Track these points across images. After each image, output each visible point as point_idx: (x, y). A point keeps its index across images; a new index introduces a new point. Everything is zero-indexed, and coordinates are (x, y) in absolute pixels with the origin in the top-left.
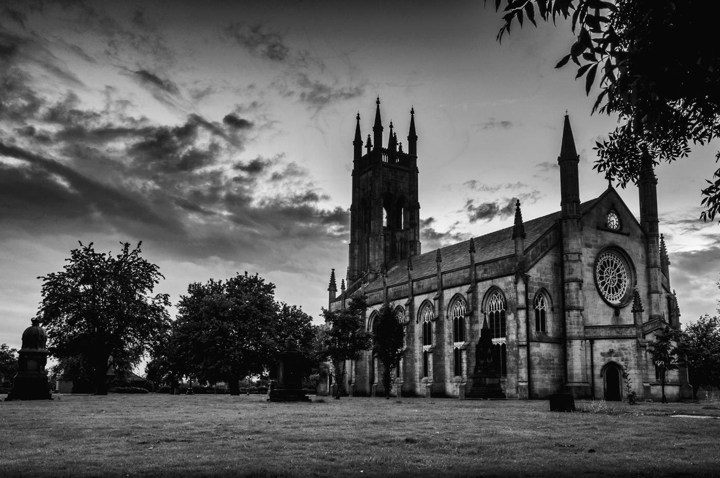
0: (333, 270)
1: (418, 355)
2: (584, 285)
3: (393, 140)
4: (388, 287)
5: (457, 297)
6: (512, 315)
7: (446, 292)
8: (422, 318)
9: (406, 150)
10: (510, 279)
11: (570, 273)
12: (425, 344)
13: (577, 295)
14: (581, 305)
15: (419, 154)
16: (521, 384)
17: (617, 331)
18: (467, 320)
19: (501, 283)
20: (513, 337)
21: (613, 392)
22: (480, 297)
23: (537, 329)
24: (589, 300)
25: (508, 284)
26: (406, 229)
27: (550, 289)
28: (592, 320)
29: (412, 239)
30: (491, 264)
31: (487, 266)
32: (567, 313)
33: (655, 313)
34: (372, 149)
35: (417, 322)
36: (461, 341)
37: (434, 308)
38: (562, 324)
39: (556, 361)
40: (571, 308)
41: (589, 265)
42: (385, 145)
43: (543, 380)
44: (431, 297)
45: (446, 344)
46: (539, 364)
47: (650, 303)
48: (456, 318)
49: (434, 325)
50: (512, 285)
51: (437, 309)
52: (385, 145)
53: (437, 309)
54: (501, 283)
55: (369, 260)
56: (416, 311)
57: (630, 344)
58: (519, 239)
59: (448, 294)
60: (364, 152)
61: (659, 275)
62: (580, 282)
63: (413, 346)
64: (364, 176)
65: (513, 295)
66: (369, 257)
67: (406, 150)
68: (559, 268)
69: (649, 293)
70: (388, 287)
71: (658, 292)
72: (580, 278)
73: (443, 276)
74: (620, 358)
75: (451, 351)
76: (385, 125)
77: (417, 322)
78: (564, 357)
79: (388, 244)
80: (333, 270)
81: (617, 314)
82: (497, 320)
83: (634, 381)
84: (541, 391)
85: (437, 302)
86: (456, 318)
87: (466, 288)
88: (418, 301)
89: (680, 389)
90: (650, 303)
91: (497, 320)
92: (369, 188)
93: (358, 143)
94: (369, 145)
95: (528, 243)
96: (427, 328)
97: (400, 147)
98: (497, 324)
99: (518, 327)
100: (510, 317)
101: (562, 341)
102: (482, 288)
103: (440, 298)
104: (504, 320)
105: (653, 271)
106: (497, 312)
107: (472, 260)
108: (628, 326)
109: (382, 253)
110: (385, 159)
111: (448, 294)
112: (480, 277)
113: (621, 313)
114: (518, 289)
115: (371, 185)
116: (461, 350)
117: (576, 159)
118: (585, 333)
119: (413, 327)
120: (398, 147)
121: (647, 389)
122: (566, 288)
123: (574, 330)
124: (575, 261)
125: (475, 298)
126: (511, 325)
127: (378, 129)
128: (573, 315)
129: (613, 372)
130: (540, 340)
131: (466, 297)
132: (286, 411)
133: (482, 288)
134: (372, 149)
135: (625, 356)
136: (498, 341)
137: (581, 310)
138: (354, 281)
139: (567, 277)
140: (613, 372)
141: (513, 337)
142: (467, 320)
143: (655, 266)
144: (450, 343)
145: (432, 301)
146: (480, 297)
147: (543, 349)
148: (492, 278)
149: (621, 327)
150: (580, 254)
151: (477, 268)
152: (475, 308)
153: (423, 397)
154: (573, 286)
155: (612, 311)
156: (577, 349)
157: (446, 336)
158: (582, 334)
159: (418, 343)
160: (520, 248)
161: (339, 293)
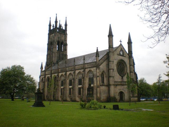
0: (97, 48)
1: (60, 89)
2: (114, 70)
3: (60, 26)
4: (59, 69)
5: (79, 73)
6: (95, 78)
7: (76, 71)
8: (69, 78)
9: (64, 28)
10: (95, 68)
11: (111, 67)
12: (70, 86)
13: (113, 73)
14: (113, 76)
15: (68, 29)
16: (98, 98)
17: (122, 84)
18: (83, 79)
19: (92, 69)
20: (95, 85)
21: (122, 100)
22: (86, 73)
23: (102, 82)
24: (115, 74)
25: (94, 70)
26: (63, 51)
27: (105, 71)
28: (116, 80)
29: (65, 54)
30: (90, 64)
31: (88, 64)
32: (110, 78)
33: (132, 78)
34: (54, 27)
35: (68, 79)
36: (71, 86)
37: (73, 75)
38: (109, 81)
39: (107, 91)
40: (111, 77)
41: (115, 65)
42: (58, 27)
43: (104, 97)
44: (72, 72)
45: (76, 86)
46: (102, 92)
47: (130, 75)
48: (79, 79)
49: (64, 81)
50: (95, 70)
51: (74, 76)
52: (58, 27)
53: (74, 76)
54: (92, 69)
55: (52, 60)
56: (60, 77)
57: (126, 86)
58: (97, 57)
59: (77, 72)
60: (52, 28)
61: (133, 68)
62: (113, 70)
63: (66, 86)
64: (52, 35)
65: (96, 73)
66: (52, 59)
67: (64, 28)
68: (108, 65)
69: (130, 72)
70: (52, 70)
71: (132, 72)
72: (113, 68)
73: (76, 66)
74: (123, 90)
75: (78, 88)
76: (58, 21)
77: (68, 79)
78: (109, 90)
79: (58, 55)
80: (97, 48)
81: (122, 78)
82: (91, 80)
83: (126, 97)
84: (103, 99)
85: (84, 72)
86: (79, 79)
87: (82, 70)
88: (68, 73)
89: (138, 98)
90: (130, 75)
91: (91, 80)
92: (53, 39)
93: (50, 25)
94: (53, 26)
95: (100, 58)
96: (71, 81)
97: (62, 27)
98: (91, 81)
99: (97, 82)
100: (95, 79)
101: (109, 86)
102: (87, 70)
103: (74, 73)
104: (93, 80)
105: (131, 66)
106: (91, 77)
107: (74, 64)
108: (125, 82)
109: (56, 58)
110: (58, 30)
111: (77, 72)
112: (86, 67)
113: (124, 78)
114: (97, 71)
115: (54, 38)
116: (81, 88)
117: (112, 36)
118: (115, 83)
119: (66, 81)
120: (62, 27)
121: (130, 99)
122: (110, 71)
123: (111, 83)
124: (112, 64)
125: (85, 73)
126: (95, 81)
127: (56, 22)
128: (111, 79)
129: (121, 94)
130: (102, 85)
131: (82, 73)
132: (85, 112)
133: (87, 70)
134: (54, 27)
135: (125, 90)
136: (92, 85)
137: (113, 77)
138: (48, 66)
139: (110, 68)
140: (121, 94)
141: (95, 85)
142: (83, 79)
143: (132, 65)
144: (77, 86)
145: (72, 74)
146: (86, 73)
147: (103, 88)
148: (90, 68)
149: (124, 82)
150: (113, 62)
151: (86, 65)
152: (85, 76)
153: (60, 101)
154: (112, 71)
155: (121, 77)
156: (112, 88)
157: (76, 84)
158: (114, 84)
159: (68, 85)
160: (98, 60)
161: (44, 69)
